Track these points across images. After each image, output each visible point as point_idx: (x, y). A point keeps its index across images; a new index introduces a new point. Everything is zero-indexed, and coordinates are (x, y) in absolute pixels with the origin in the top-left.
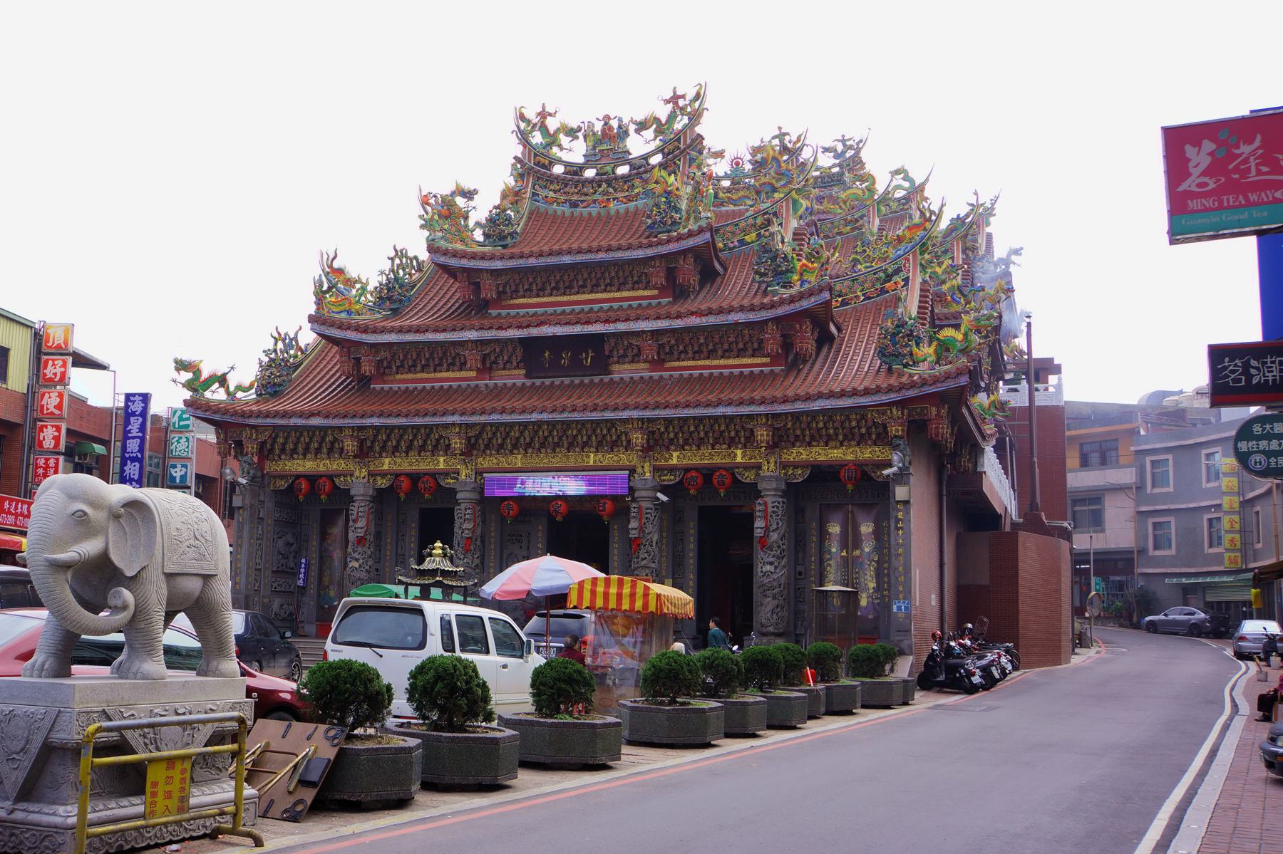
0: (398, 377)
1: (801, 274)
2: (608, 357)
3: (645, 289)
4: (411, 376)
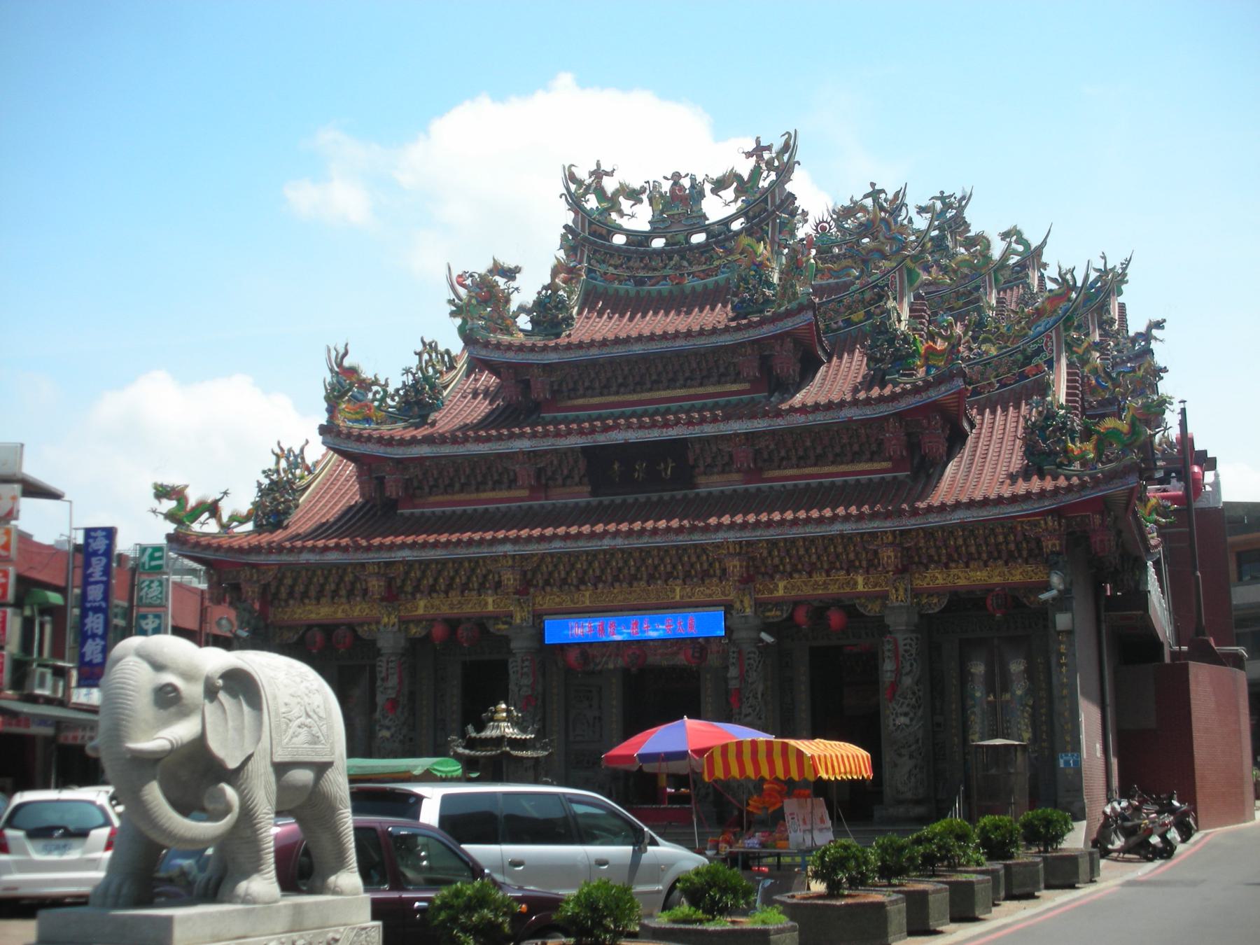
0: (432, 499)
1: (927, 359)
2: (693, 467)
3: (734, 382)
4: (448, 498)
